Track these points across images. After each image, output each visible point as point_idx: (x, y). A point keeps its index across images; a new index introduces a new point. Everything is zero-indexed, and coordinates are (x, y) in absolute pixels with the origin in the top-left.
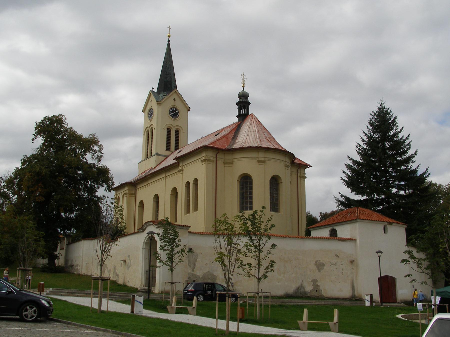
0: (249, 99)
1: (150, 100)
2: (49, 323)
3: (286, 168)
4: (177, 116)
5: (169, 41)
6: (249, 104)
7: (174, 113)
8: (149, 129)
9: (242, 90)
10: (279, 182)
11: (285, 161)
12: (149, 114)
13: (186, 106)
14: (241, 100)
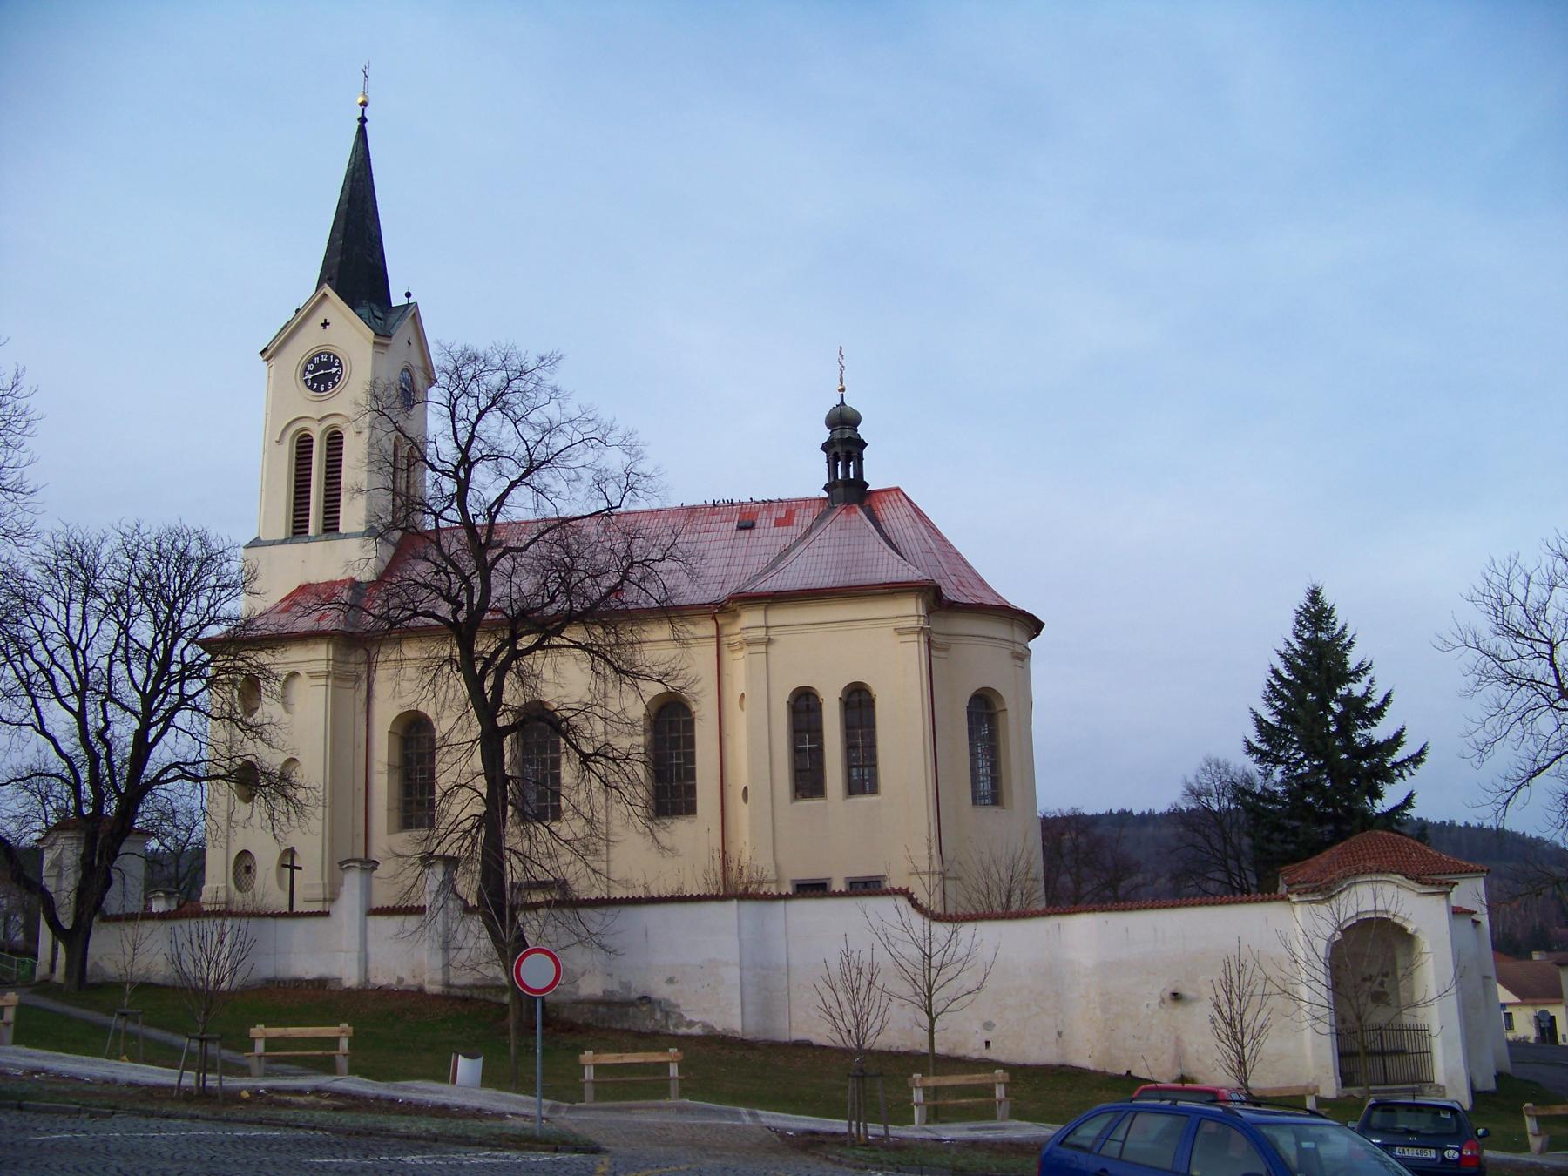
0: (863, 431)
1: (318, 318)
2: (453, 991)
3: (1019, 663)
4: (336, 380)
5: (363, 120)
10: (998, 709)
11: (1014, 642)
14: (837, 435)
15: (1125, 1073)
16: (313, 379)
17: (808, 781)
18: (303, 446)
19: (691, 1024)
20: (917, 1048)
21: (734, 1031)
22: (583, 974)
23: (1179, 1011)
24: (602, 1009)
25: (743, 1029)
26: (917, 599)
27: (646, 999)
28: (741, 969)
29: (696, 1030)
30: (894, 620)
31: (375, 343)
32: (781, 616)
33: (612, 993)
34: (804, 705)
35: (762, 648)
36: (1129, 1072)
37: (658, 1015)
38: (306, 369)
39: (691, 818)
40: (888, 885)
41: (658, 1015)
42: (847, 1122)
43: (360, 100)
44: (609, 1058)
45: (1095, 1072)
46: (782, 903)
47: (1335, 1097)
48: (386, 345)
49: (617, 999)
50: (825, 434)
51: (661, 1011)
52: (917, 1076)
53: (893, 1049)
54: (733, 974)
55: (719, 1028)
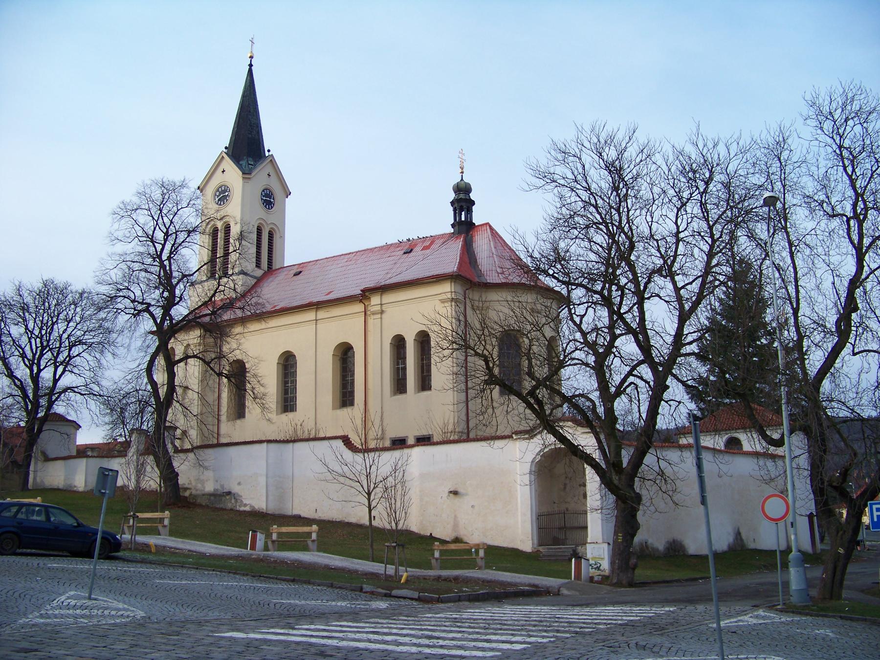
0: (473, 196)
1: (220, 169)
5: (251, 65)
6: (473, 203)
7: (268, 200)
8: (219, 225)
9: (460, 179)
12: (217, 194)
13: (281, 182)
15: (429, 534)
16: (219, 200)
17: (400, 386)
18: (215, 233)
19: (245, 505)
20: (344, 519)
21: (263, 509)
22: (207, 481)
23: (456, 500)
24: (212, 498)
25: (266, 508)
26: (451, 282)
27: (229, 493)
28: (267, 477)
29: (247, 509)
30: (439, 296)
31: (243, 178)
32: (389, 298)
33: (217, 490)
34: (399, 343)
35: (379, 316)
36: (431, 534)
37: (233, 501)
38: (216, 195)
39: (352, 407)
40: (435, 439)
41: (233, 501)
42: (384, 565)
43: (249, 55)
44: (284, 529)
45: (417, 533)
46: (291, 444)
47: (531, 551)
48: (249, 178)
49: (219, 493)
50: (452, 196)
51: (234, 498)
52: (275, 526)
53: (334, 520)
54: (262, 480)
55: (256, 507)
